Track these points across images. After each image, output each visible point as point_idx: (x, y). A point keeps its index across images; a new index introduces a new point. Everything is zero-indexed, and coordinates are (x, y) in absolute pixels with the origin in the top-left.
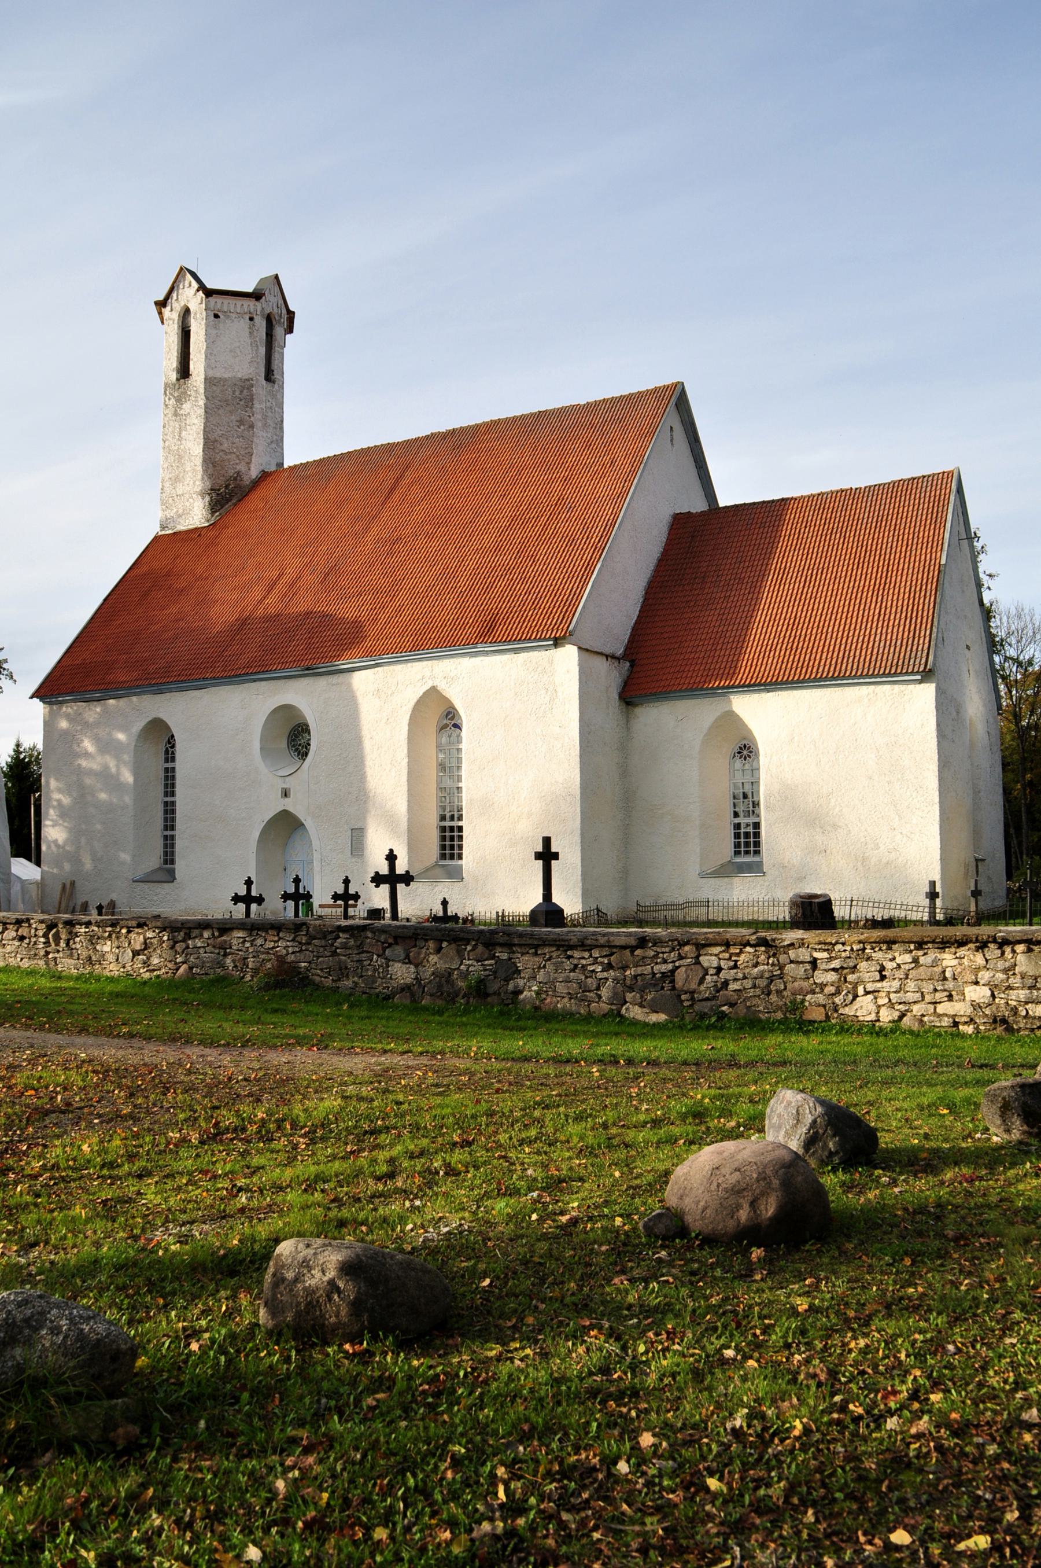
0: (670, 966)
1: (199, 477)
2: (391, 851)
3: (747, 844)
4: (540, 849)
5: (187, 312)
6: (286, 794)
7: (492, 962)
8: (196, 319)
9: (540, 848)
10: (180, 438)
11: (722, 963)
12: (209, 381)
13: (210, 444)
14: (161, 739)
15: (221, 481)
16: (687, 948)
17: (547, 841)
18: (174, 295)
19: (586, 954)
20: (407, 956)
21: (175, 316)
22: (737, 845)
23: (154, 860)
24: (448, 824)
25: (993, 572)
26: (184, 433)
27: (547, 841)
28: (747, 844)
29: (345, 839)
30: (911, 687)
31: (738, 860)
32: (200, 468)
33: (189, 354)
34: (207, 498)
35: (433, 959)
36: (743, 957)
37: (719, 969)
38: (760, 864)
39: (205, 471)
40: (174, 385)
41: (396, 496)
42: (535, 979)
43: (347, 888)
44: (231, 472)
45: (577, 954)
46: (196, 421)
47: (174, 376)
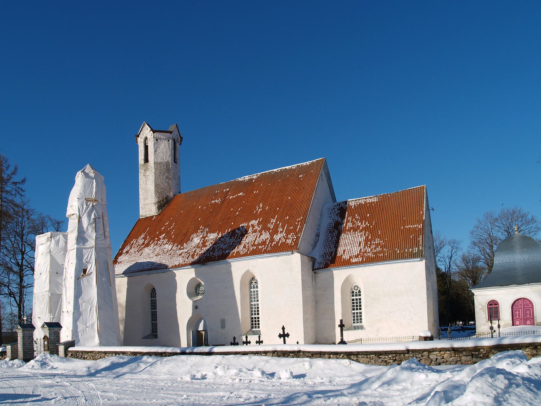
5: (146, 138)
11: (438, 357)
13: (157, 186)
16: (425, 353)
18: (142, 132)
19: (387, 357)
21: (143, 140)
23: (149, 332)
24: (359, 311)
25: (23, 179)
27: (341, 321)
28: (357, 320)
30: (416, 263)
32: (154, 195)
33: (148, 154)
34: (157, 206)
36: (445, 355)
37: (437, 359)
43: (259, 339)
45: (383, 357)
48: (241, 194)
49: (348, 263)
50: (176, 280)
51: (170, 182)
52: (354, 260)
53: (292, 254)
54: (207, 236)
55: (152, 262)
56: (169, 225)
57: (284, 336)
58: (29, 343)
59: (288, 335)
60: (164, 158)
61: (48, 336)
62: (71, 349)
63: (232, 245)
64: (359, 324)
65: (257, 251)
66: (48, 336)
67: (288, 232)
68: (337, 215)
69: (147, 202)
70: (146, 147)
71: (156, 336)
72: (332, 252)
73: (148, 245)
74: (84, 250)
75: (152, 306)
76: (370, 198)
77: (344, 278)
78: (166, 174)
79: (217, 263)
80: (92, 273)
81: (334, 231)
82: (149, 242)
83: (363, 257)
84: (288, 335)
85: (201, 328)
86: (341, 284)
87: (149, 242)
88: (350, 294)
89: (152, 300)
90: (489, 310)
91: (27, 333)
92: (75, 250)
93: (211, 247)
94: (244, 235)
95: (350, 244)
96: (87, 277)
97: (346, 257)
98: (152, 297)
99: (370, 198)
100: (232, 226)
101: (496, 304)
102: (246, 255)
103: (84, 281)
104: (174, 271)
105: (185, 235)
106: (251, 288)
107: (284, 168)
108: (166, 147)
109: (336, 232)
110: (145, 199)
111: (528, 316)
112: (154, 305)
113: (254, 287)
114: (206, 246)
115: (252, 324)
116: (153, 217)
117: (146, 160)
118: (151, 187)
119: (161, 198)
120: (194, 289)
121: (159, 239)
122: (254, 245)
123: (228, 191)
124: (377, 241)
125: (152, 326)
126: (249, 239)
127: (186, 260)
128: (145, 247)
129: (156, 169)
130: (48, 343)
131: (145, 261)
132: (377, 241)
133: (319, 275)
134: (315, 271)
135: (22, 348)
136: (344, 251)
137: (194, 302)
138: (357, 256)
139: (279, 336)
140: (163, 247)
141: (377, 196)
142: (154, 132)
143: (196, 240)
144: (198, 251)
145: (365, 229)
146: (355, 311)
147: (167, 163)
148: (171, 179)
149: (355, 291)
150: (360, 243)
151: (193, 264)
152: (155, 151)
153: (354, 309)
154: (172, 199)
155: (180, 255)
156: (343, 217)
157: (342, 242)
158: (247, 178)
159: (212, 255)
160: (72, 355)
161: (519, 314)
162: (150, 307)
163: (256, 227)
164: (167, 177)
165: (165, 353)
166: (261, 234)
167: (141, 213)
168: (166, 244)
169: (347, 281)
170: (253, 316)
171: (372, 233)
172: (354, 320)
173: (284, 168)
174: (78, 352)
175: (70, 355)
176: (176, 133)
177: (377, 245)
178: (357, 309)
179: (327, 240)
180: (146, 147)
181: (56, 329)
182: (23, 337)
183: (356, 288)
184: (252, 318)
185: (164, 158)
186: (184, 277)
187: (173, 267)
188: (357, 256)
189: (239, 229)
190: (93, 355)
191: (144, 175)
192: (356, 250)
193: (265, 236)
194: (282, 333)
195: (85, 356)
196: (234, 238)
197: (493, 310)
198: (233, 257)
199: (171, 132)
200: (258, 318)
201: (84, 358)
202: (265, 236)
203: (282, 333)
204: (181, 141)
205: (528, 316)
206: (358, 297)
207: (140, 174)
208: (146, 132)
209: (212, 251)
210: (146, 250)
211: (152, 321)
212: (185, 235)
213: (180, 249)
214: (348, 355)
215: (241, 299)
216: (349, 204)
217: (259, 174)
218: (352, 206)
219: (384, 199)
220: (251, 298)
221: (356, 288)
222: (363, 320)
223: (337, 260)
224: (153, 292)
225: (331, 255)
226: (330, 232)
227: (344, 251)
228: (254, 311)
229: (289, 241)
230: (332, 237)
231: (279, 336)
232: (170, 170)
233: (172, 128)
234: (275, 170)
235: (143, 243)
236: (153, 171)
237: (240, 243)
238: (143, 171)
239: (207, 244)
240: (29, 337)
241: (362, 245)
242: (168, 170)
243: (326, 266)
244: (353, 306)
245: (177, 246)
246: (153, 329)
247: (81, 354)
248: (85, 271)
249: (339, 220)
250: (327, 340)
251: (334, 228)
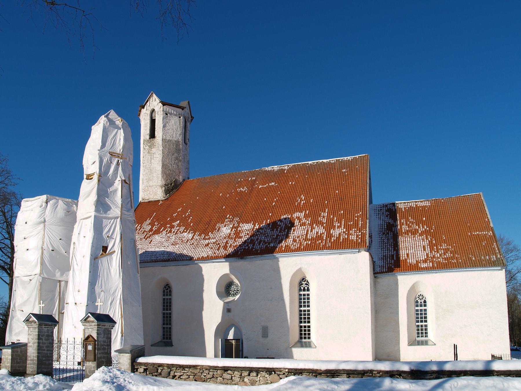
1: (160, 179)
3: (167, 306)
5: (153, 111)
8: (158, 114)
10: (151, 163)
13: (164, 166)
18: (148, 103)
23: (159, 338)
24: (424, 324)
26: (152, 161)
31: (418, 339)
32: (160, 176)
34: (163, 189)
38: (310, 342)
39: (162, 177)
40: (148, 141)
42: (403, 375)
46: (158, 156)
47: (148, 137)
48: (273, 184)
49: (415, 268)
50: (202, 276)
51: (180, 164)
52: (424, 265)
53: (359, 252)
54: (239, 226)
55: (168, 252)
56: (184, 211)
58: (47, 347)
60: (174, 136)
61: (95, 336)
62: (141, 360)
63: (277, 238)
64: (424, 339)
65: (313, 246)
66: (95, 336)
67: (348, 228)
68: (387, 216)
69: (151, 183)
70: (153, 122)
71: (170, 344)
72: (393, 256)
73: (157, 232)
74: (104, 220)
75: (164, 306)
76: (421, 202)
77: (411, 285)
78: (176, 155)
79: (260, 257)
80: (115, 252)
81: (388, 233)
82: (159, 229)
83: (432, 262)
85: (231, 336)
86: (406, 292)
87: (159, 229)
88: (413, 304)
89: (164, 299)
91: (45, 329)
92: (92, 220)
93: (248, 239)
94: (290, 229)
95: (412, 246)
96: (108, 257)
97: (412, 261)
98: (164, 295)
99: (421, 202)
100: (270, 218)
102: (298, 250)
103: (104, 261)
104: (201, 265)
105: (208, 223)
106: (300, 290)
107: (321, 161)
108: (176, 124)
109: (391, 235)
110: (149, 180)
112: (167, 305)
113: (304, 290)
114: (241, 237)
115: (301, 334)
116: (158, 201)
117: (152, 135)
118: (157, 166)
119: (169, 181)
120: (226, 288)
121: (172, 227)
122: (306, 239)
123: (255, 180)
124: (444, 246)
125: (164, 332)
126: (297, 232)
127: (217, 252)
128: (154, 234)
129: (164, 147)
130: (94, 348)
131: (157, 250)
132: (444, 246)
133: (379, 280)
134: (376, 275)
135: (36, 354)
136: (408, 255)
137: (226, 303)
138: (425, 261)
140: (179, 235)
141: (428, 201)
142: (164, 104)
143: (225, 230)
144: (231, 242)
145: (425, 233)
146: (420, 324)
147: (177, 143)
148: (180, 161)
150: (424, 247)
151: (227, 257)
152: (164, 126)
153: (418, 322)
154: (181, 184)
155: (207, 245)
156: (395, 220)
157: (401, 245)
158: (276, 168)
159: (252, 248)
160: (145, 370)
162: (161, 307)
163: (304, 220)
164: (177, 158)
165: (371, 371)
166: (312, 228)
168: (183, 232)
169: (413, 288)
170: (303, 324)
171: (435, 239)
172: (418, 333)
173: (321, 161)
174: (160, 365)
175: (141, 370)
176: (187, 110)
177: (446, 251)
178: (422, 321)
179: (382, 242)
180: (153, 122)
181: (107, 325)
182: (39, 335)
183: (421, 297)
184: (301, 327)
185: (174, 136)
186: (214, 272)
187: (199, 259)
188: (425, 261)
189: (281, 221)
190: (196, 371)
191: (149, 153)
192: (422, 255)
193: (319, 230)
195: (178, 374)
196: (277, 230)
198: (281, 251)
199: (183, 108)
200: (309, 327)
201: (174, 377)
202: (319, 230)
204: (192, 120)
206: (423, 308)
208: (154, 102)
209: (250, 243)
210: (157, 238)
211: (164, 324)
212: (208, 223)
213: (204, 239)
214: (348, 374)
215: (290, 303)
216: (398, 207)
217: (291, 165)
218: (402, 209)
219: (436, 205)
220: (300, 302)
221: (421, 297)
222: (429, 334)
223: (402, 264)
224: (167, 289)
225: (393, 258)
226: (384, 233)
227: (408, 255)
228: (304, 317)
229: (353, 237)
230: (388, 239)
232: (180, 150)
233: (184, 104)
234: (310, 162)
235: (151, 230)
236: (161, 148)
237: (287, 236)
239: (242, 235)
240: (48, 336)
241: (428, 250)
242: (178, 150)
243: (390, 270)
244: (417, 318)
245: (200, 235)
246: (164, 335)
247: (166, 370)
248: (105, 249)
249: (391, 221)
250: (388, 356)
251: (387, 229)
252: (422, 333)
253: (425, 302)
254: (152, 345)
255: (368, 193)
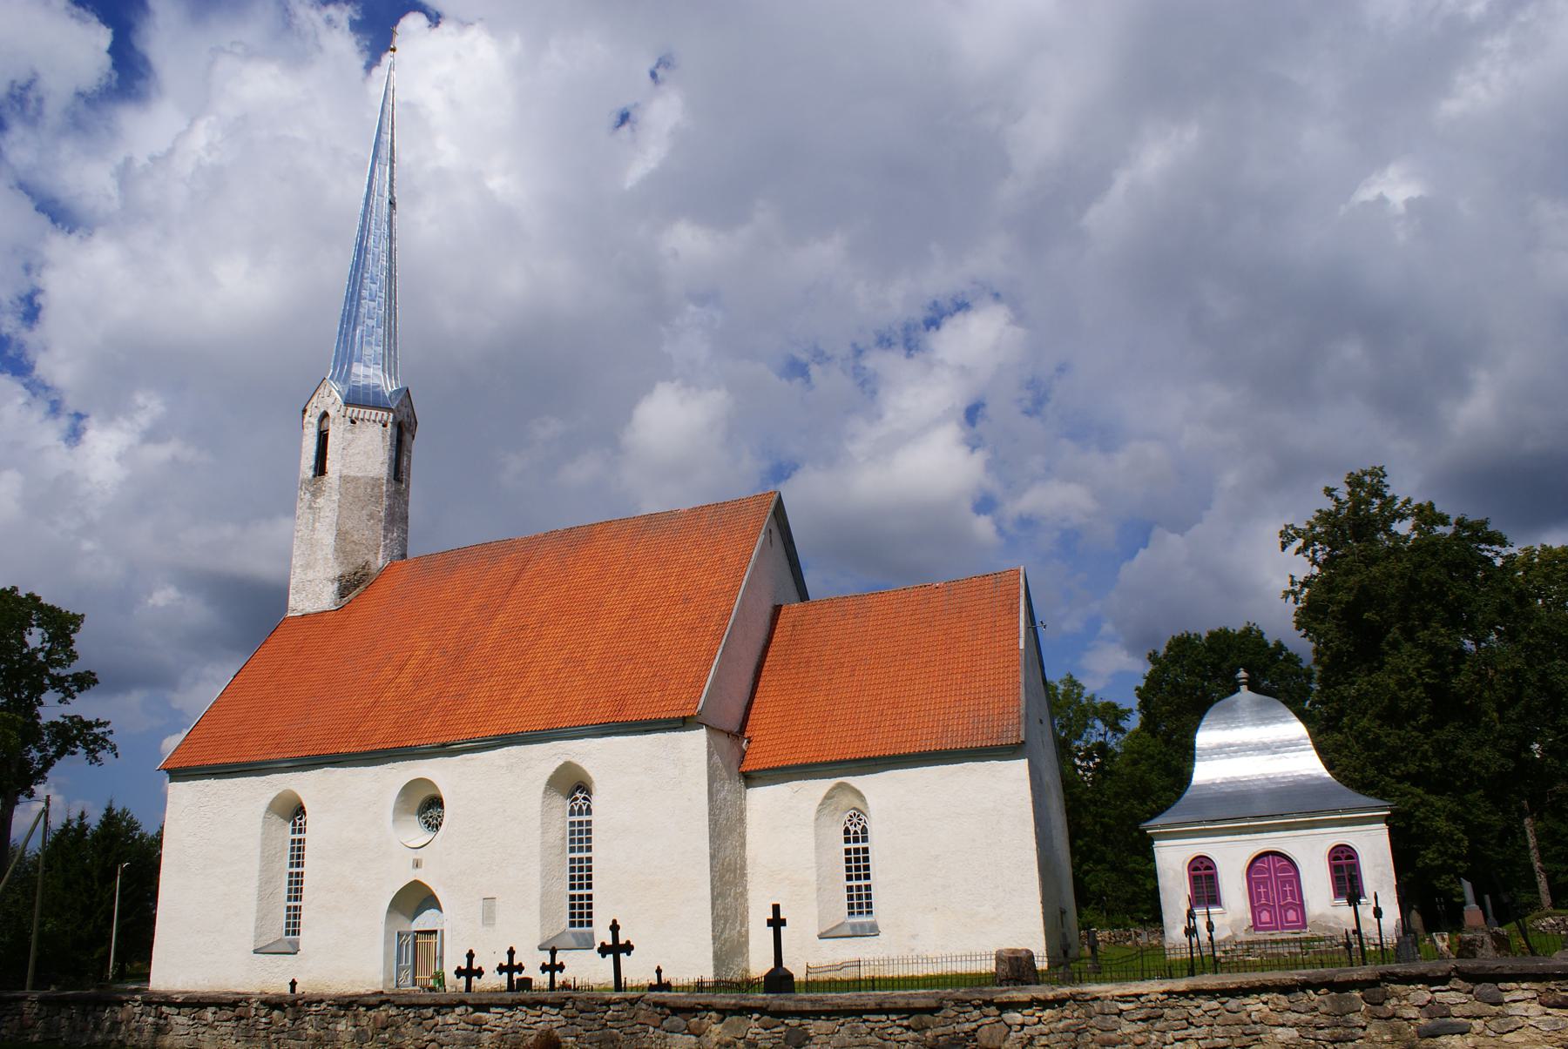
0: (974, 1025)
2: (614, 921)
4: (771, 916)
5: (325, 415)
6: (417, 864)
7: (782, 1029)
9: (771, 916)
10: (313, 530)
12: (344, 479)
13: (341, 535)
14: (573, 786)
15: (351, 569)
17: (776, 908)
19: (884, 1017)
20: (687, 1027)
21: (315, 421)
22: (851, 906)
24: (863, 883)
27: (776, 908)
29: (477, 909)
35: (717, 1028)
41: (519, 586)
44: (360, 561)
45: (872, 1018)
57: (617, 949)
59: (628, 948)
64: (864, 919)
70: (323, 438)
84: (628, 948)
90: (1194, 880)
101: (1208, 868)
104: (1328, 775)
110: (307, 566)
111: (1289, 899)
117: (320, 468)
139: (632, 948)
147: (375, 482)
149: (852, 829)
161: (1266, 893)
167: (292, 603)
183: (855, 820)
191: (310, 507)
194: (464, 966)
197: (1203, 877)
200: (849, 878)
203: (464, 966)
205: (1289, 899)
207: (300, 504)
221: (855, 820)
231: (632, 948)
236: (336, 497)
238: (308, 496)
252: (860, 905)
253: (864, 830)
254: (256, 952)
255: (1022, 608)
